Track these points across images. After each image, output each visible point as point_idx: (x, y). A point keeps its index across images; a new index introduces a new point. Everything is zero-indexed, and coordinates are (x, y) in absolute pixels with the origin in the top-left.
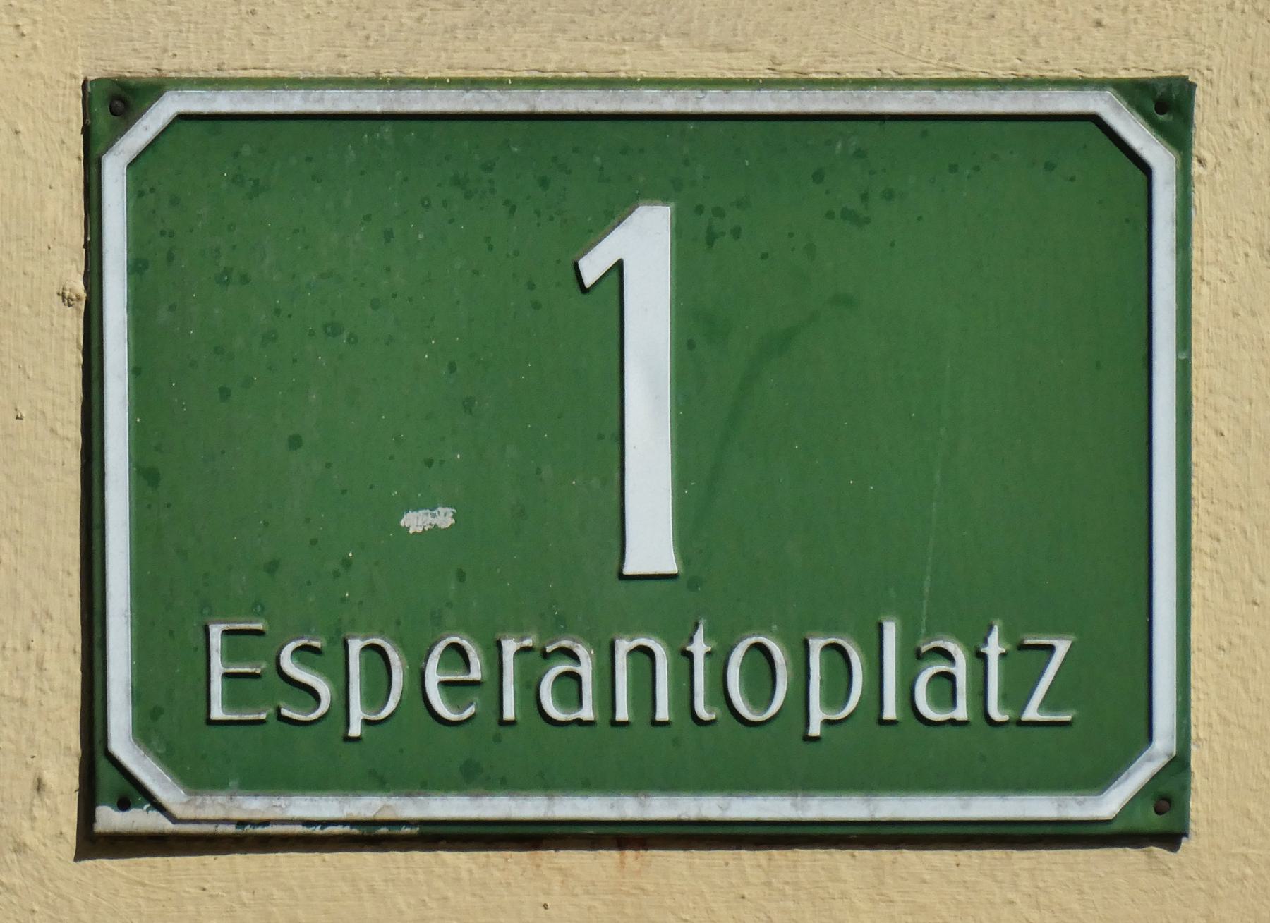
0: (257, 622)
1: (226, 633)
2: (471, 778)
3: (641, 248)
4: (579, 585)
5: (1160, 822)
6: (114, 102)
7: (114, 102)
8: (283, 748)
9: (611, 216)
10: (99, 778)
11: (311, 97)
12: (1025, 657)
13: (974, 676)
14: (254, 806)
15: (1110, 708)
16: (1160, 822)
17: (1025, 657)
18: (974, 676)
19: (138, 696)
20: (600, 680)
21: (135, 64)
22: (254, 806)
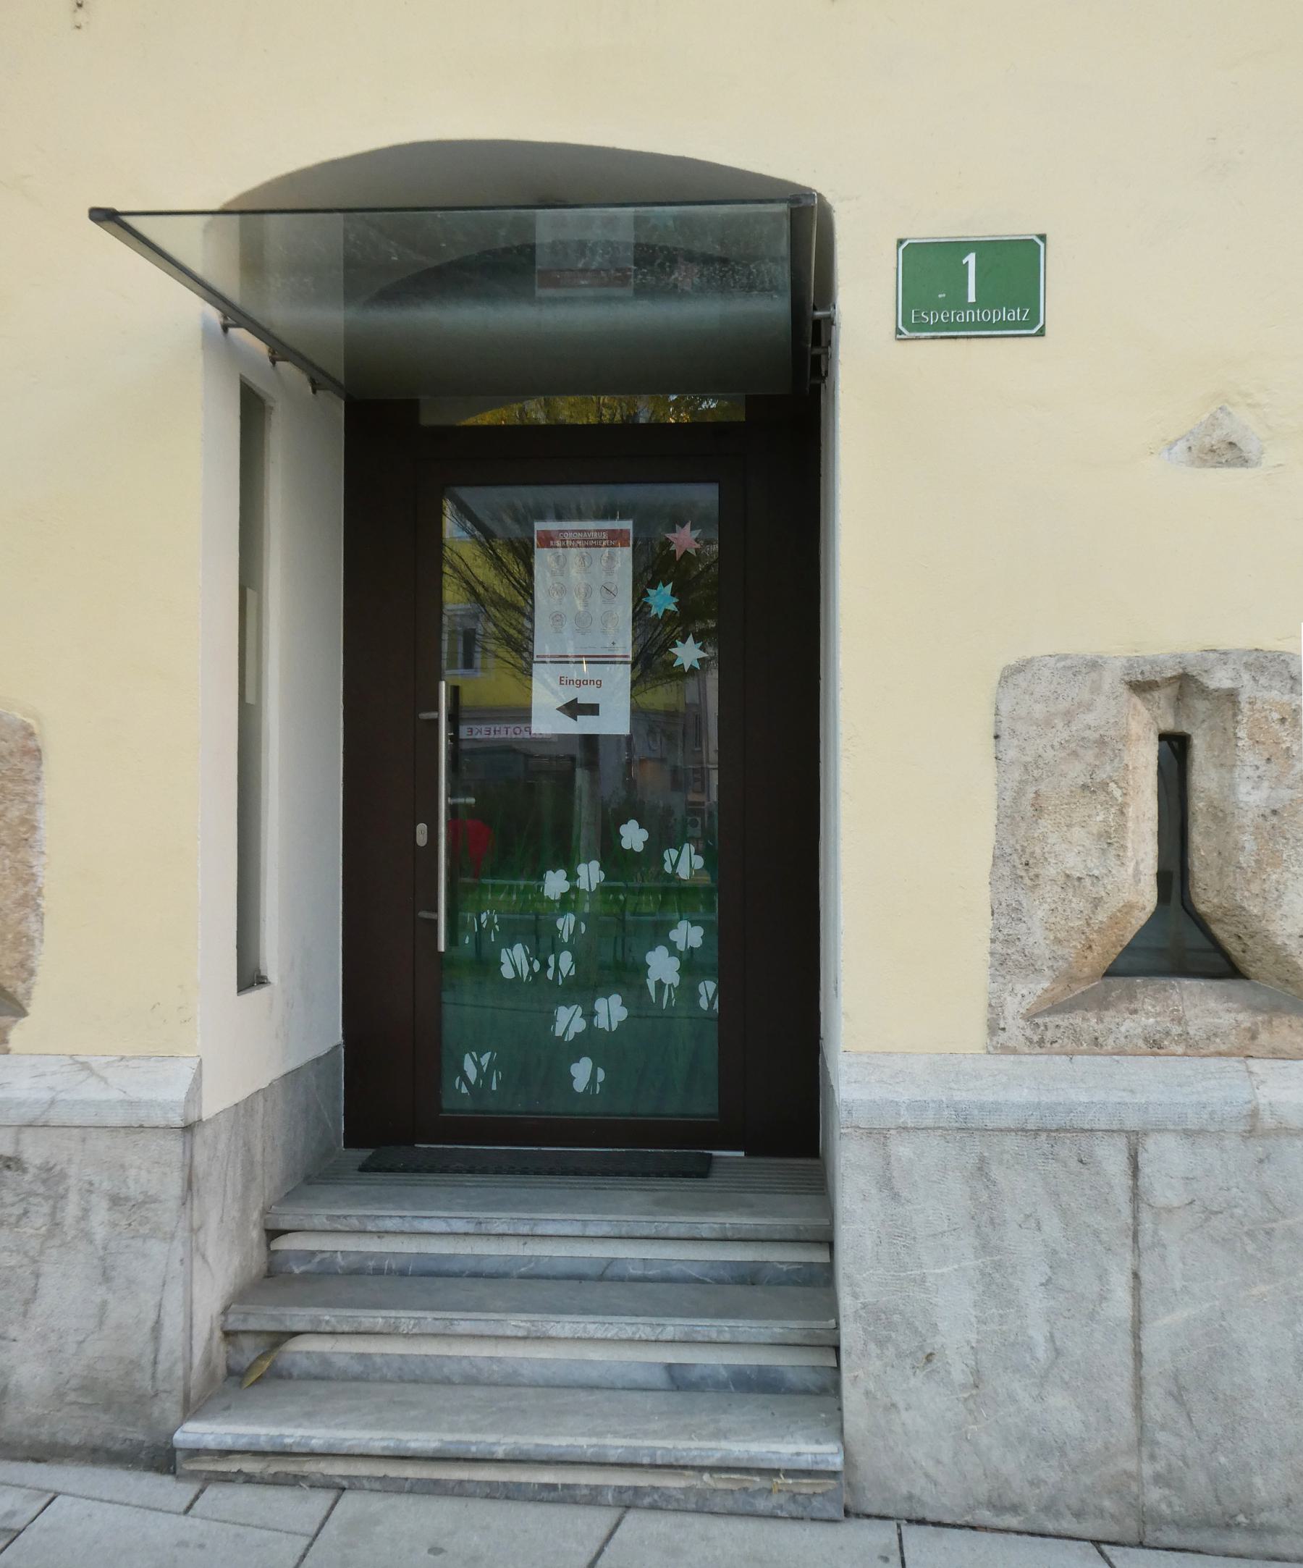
0: (482, 410)
1: (627, 531)
2: (947, 330)
3: (971, 259)
4: (962, 304)
5: (1041, 333)
6: (901, 242)
7: (901, 242)
8: (926, 327)
9: (967, 254)
10: (899, 332)
11: (810, 1458)
12: (1022, 312)
13: (1015, 315)
14: (918, 334)
15: (1033, 319)
16: (1041, 333)
17: (1022, 312)
18: (1015, 315)
19: (448, 823)
20: (964, 316)
21: (902, 236)
22: (918, 334)
